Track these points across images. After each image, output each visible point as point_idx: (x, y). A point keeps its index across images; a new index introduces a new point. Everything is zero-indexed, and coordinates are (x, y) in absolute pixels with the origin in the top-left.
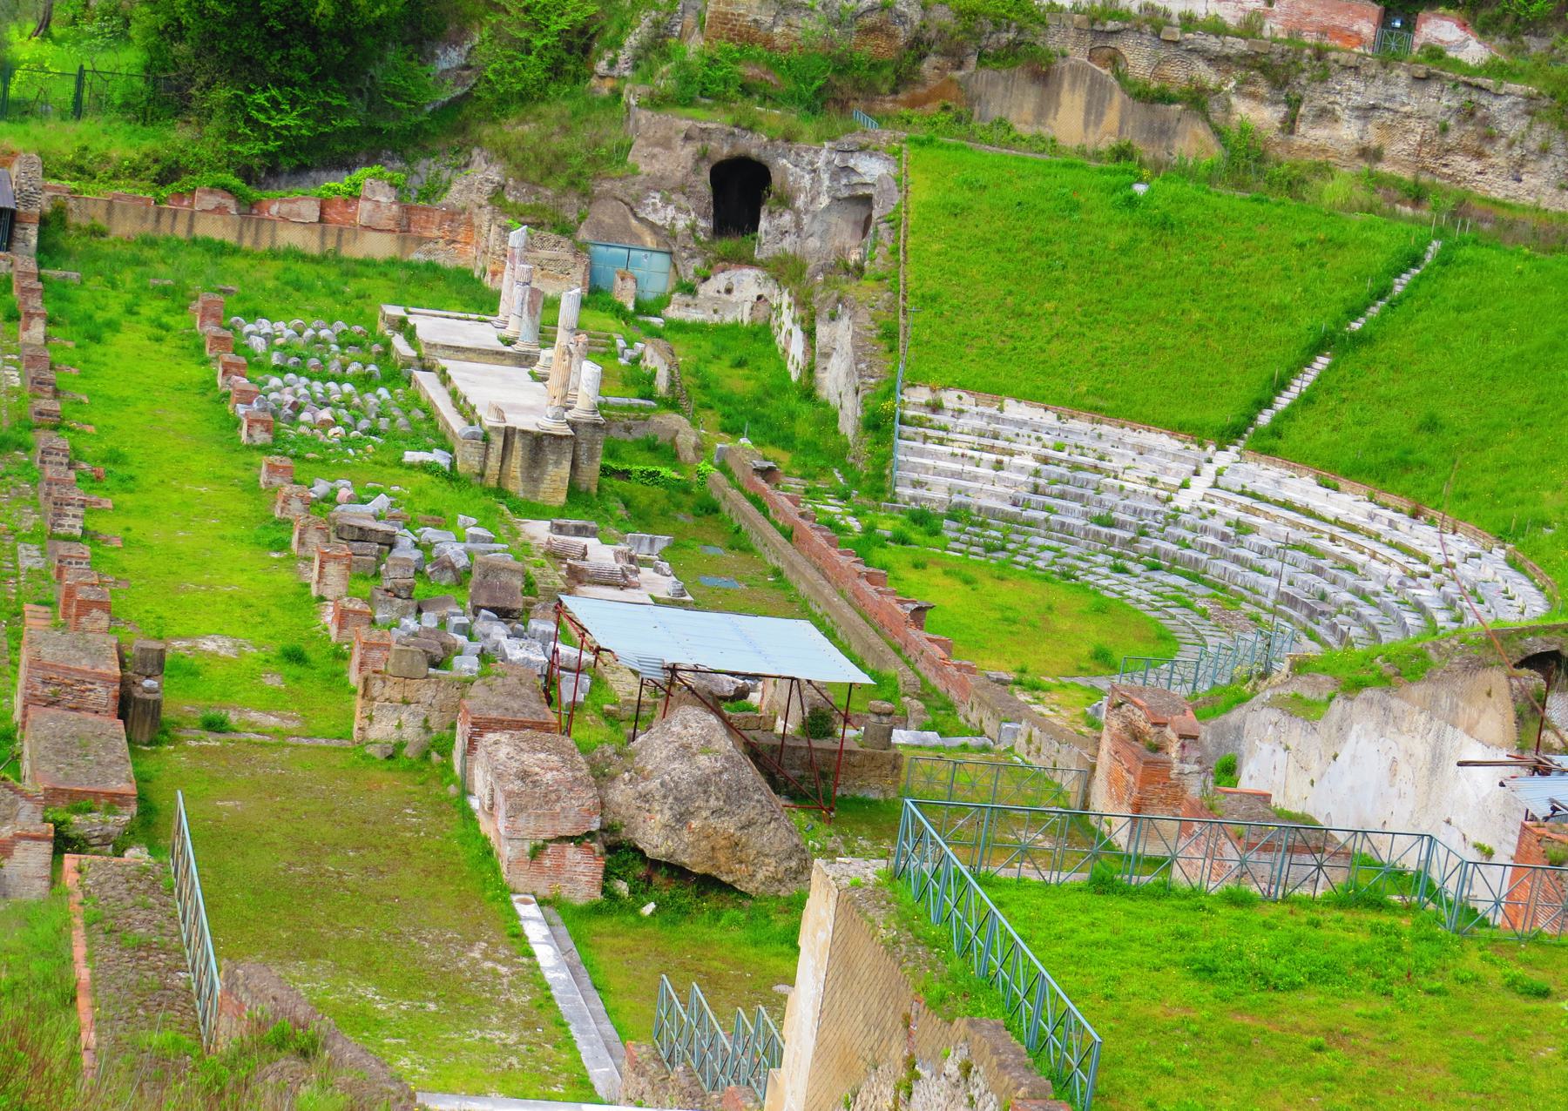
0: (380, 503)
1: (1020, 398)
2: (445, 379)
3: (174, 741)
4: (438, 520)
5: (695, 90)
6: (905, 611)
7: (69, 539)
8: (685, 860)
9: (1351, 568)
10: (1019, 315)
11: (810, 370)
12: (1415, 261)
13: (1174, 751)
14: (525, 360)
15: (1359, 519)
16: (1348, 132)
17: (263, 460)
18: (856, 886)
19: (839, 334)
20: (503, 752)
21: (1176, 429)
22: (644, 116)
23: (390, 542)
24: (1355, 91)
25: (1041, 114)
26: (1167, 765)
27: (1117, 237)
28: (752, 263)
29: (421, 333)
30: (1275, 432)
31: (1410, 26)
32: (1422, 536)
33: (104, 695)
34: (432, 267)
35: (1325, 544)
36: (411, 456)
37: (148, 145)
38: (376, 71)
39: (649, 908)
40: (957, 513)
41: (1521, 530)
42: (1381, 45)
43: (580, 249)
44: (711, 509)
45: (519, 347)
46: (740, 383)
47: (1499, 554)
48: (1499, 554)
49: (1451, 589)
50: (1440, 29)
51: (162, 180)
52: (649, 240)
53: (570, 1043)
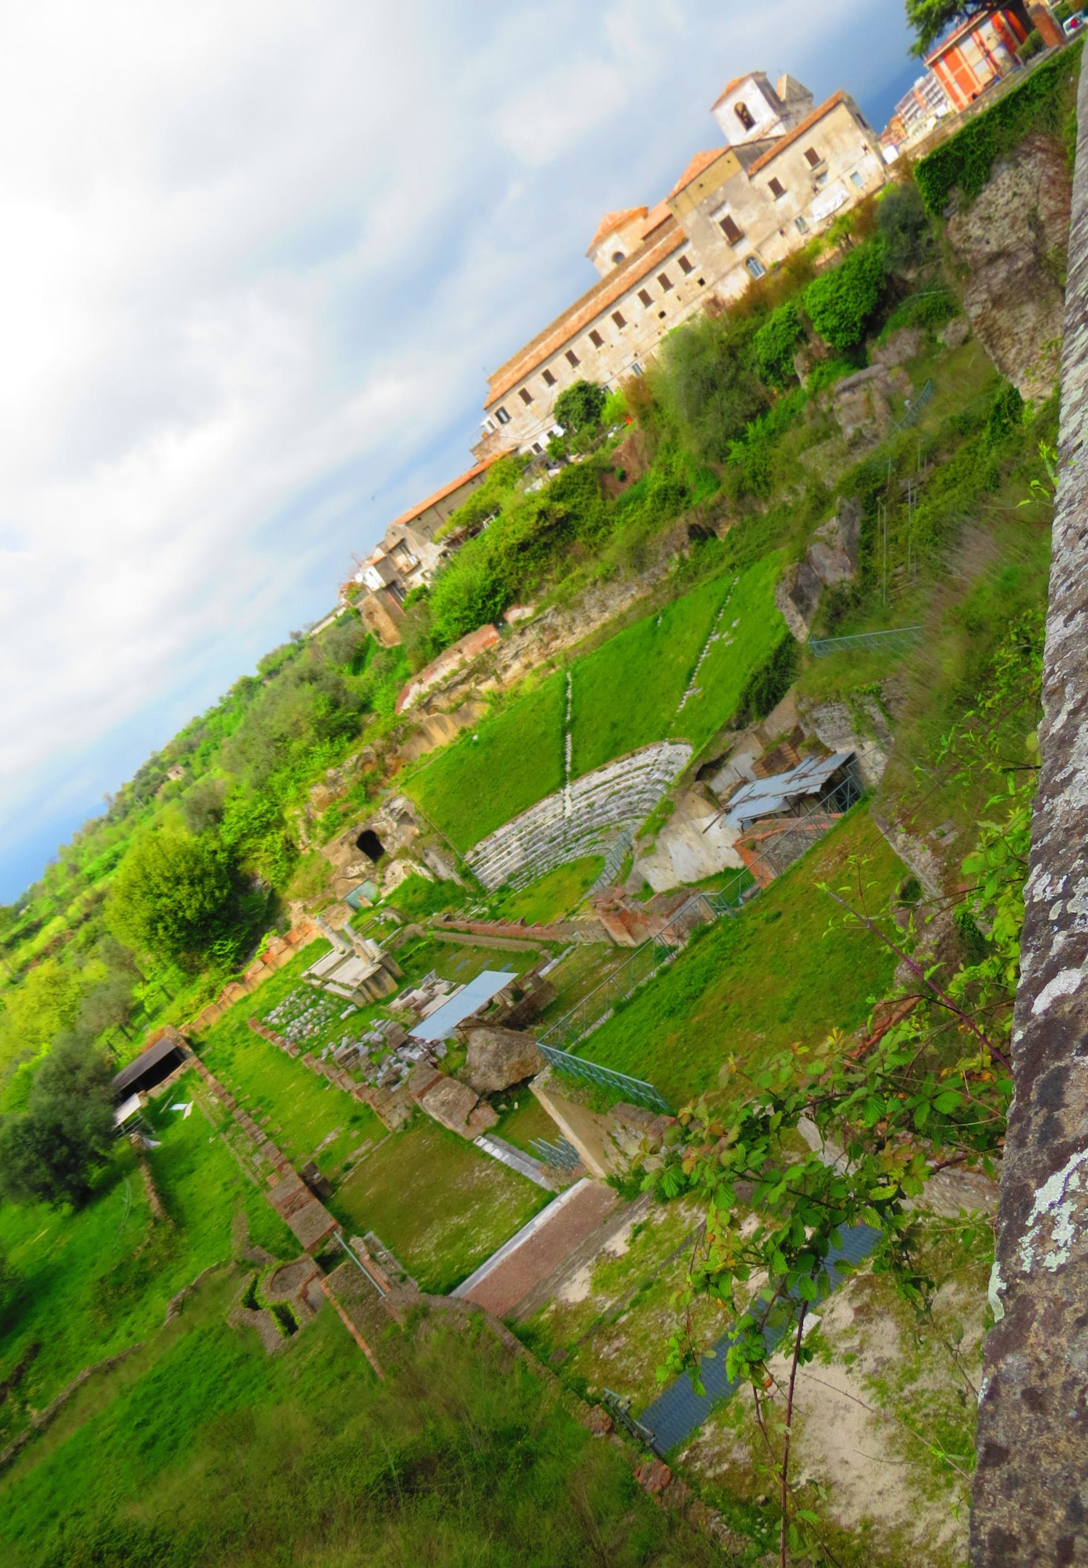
0: (345, 1040)
1: (497, 829)
2: (334, 982)
3: (339, 1185)
4: (366, 1029)
5: (331, 829)
6: (518, 926)
7: (265, 1142)
8: (512, 1081)
9: (630, 787)
10: (475, 805)
11: (435, 876)
12: (567, 684)
13: (623, 906)
14: (352, 954)
15: (620, 771)
16: (516, 666)
17: (302, 1059)
18: (546, 1084)
19: (432, 858)
20: (431, 1101)
21: (547, 795)
22: (324, 849)
23: (356, 1051)
24: (508, 653)
25: (431, 743)
26: (625, 911)
27: (482, 756)
28: (392, 860)
29: (318, 974)
30: (574, 769)
31: (504, 621)
32: (642, 759)
33: (305, 1194)
34: (308, 947)
35: (617, 788)
36: (343, 1016)
37: (198, 990)
38: (241, 907)
39: (516, 1105)
40: (511, 877)
41: (665, 732)
42: (501, 635)
43: (342, 903)
44: (442, 945)
45: (348, 951)
46: (420, 898)
47: (666, 744)
48: (666, 744)
49: (662, 768)
50: (514, 615)
51: (211, 996)
52: (359, 881)
53: (527, 1180)
